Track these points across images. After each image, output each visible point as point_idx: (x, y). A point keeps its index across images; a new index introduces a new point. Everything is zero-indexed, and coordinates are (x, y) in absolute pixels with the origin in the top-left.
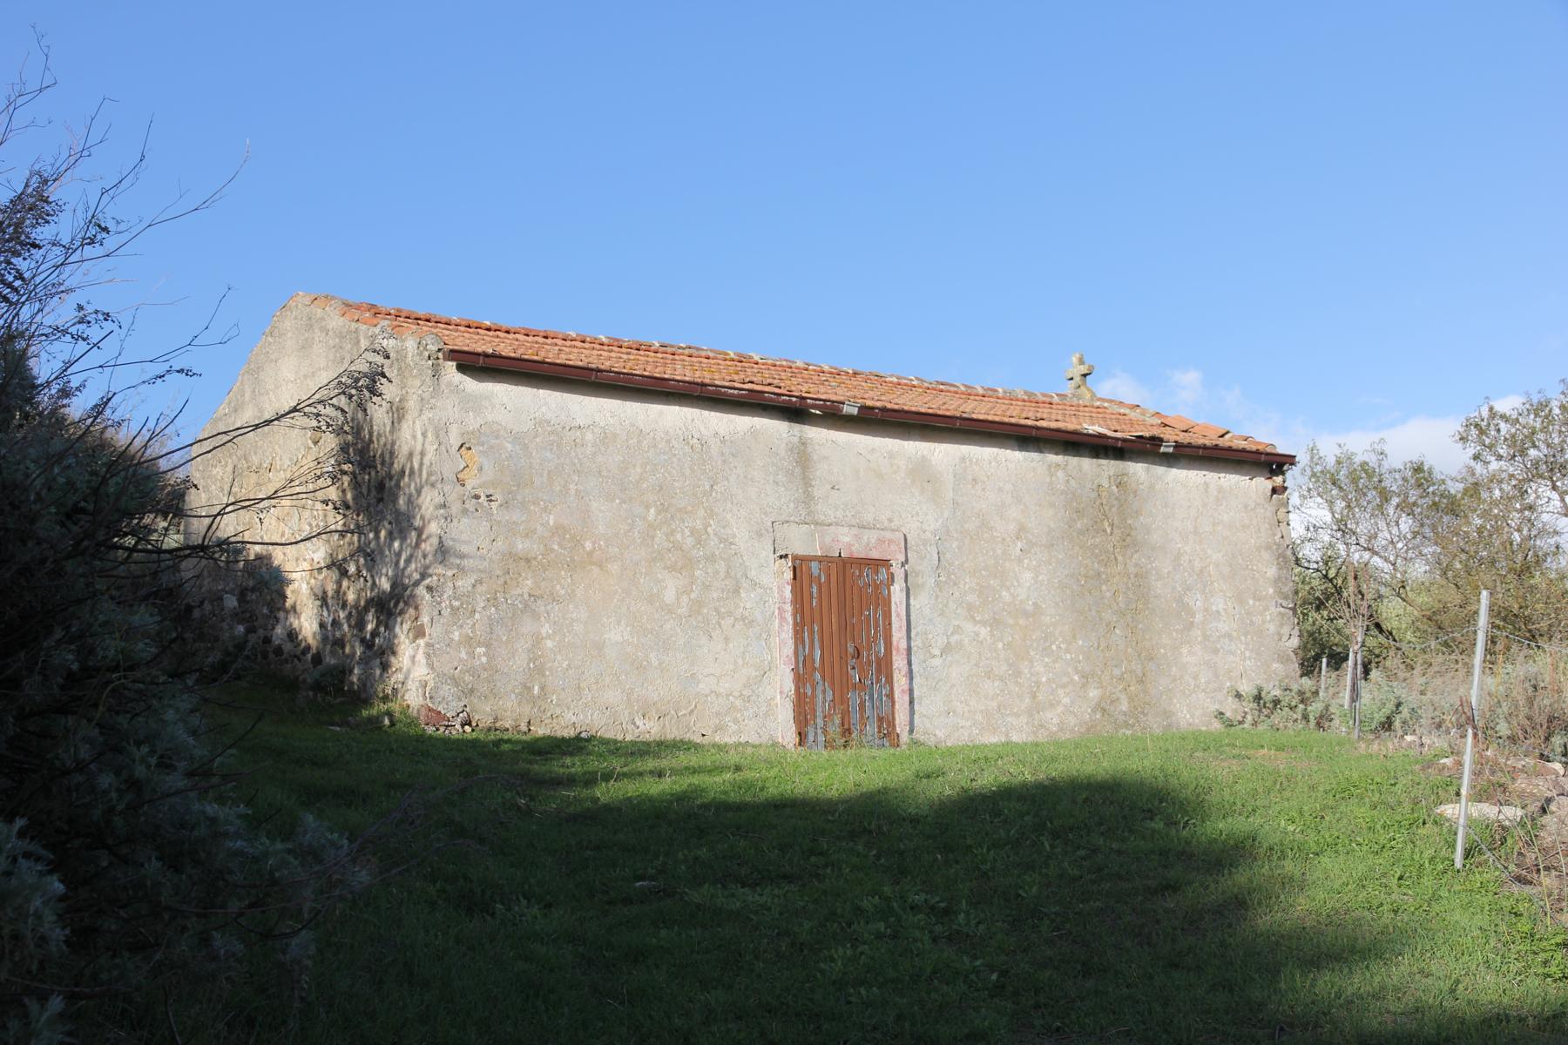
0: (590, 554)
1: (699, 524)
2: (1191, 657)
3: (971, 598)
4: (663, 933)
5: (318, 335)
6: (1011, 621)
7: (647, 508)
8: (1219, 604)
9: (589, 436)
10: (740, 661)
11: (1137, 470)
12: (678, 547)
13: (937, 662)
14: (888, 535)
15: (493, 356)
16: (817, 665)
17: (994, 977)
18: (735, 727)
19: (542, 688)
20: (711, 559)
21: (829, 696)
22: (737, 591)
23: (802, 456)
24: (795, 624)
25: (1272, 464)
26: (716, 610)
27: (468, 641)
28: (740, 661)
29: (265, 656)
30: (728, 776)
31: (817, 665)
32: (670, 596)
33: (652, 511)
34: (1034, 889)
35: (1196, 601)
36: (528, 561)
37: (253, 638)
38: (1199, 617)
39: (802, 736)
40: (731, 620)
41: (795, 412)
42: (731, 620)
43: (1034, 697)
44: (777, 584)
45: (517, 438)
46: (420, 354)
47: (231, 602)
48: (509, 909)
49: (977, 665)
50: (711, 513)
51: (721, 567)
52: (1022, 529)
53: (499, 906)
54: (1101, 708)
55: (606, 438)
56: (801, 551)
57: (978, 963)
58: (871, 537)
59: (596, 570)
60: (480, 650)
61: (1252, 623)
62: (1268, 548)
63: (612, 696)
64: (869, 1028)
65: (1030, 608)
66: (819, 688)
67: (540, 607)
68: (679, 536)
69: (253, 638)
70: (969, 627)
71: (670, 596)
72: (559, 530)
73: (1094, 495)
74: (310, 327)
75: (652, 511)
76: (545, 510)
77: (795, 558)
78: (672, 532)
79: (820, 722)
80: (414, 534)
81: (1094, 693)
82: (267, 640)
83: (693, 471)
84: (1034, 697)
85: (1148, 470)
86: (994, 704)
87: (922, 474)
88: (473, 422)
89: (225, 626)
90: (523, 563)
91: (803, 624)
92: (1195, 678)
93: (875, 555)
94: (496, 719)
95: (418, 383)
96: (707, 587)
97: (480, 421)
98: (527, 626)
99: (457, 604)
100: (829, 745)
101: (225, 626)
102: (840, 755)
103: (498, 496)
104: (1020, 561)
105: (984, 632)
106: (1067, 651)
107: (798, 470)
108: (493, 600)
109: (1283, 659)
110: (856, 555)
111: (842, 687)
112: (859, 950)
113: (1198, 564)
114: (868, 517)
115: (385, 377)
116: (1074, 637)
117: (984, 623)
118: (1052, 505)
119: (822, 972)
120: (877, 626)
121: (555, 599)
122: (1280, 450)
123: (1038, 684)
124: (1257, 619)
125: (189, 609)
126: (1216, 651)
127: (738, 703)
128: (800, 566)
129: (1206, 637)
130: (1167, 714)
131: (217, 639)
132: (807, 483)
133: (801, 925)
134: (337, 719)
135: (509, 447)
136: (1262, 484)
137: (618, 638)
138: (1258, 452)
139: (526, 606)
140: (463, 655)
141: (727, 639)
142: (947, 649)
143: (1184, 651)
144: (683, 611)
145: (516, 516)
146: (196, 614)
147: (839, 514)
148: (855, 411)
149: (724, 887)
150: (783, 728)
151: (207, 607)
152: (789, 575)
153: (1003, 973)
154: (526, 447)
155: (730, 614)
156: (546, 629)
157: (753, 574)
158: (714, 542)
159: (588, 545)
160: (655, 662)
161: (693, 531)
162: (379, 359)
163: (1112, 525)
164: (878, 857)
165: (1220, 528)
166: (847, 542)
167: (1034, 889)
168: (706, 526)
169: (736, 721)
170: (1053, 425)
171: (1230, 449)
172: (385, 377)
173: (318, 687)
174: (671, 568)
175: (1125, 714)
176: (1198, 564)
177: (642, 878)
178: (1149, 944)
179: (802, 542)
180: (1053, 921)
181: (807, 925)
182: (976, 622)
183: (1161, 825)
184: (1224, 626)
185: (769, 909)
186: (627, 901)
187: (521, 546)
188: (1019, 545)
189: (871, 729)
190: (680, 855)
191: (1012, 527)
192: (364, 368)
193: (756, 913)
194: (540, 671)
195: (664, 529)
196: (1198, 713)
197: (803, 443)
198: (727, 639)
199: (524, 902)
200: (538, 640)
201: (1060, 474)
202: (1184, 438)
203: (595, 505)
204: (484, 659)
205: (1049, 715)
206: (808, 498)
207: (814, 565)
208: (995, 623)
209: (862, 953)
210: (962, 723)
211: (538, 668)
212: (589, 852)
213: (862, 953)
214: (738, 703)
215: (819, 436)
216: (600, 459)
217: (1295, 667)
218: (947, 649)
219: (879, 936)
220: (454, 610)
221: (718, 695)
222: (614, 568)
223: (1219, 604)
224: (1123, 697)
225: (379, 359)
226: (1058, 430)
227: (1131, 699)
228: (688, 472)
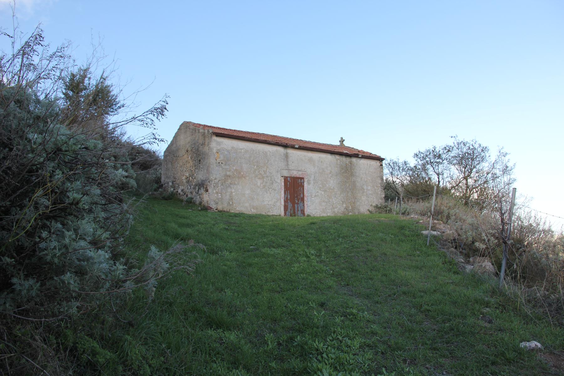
0: (243, 175)
1: (265, 170)
2: (364, 198)
3: (321, 186)
4: (256, 259)
5: (188, 129)
6: (328, 190)
7: (254, 166)
8: (369, 188)
9: (243, 151)
10: (273, 198)
11: (354, 160)
12: (261, 174)
13: (313, 199)
14: (304, 172)
15: (223, 134)
16: (289, 199)
17: (331, 272)
18: (272, 212)
19: (232, 203)
20: (267, 177)
21: (291, 205)
22: (272, 183)
23: (287, 156)
24: (284, 190)
25: (381, 160)
26: (268, 187)
27: (217, 193)
28: (273, 198)
29: (177, 195)
30: (271, 223)
31: (289, 199)
32: (259, 184)
33: (255, 166)
34: (339, 250)
35: (365, 187)
36: (229, 176)
37: (174, 191)
38: (365, 190)
39: (285, 213)
40: (271, 189)
41: (286, 146)
42: (271, 189)
43: (333, 206)
44: (281, 183)
45: (228, 151)
46: (208, 133)
47: (170, 184)
48: (222, 253)
49: (321, 199)
50: (267, 167)
51: (269, 178)
52: (331, 172)
53: (220, 252)
54: (346, 208)
55: (246, 151)
56: (286, 175)
57: (328, 268)
58: (300, 173)
59: (243, 178)
60: (219, 195)
61: (376, 192)
62: (379, 177)
63: (247, 205)
64: (304, 285)
65: (332, 188)
66: (289, 204)
67: (232, 186)
68: (261, 172)
69: (174, 191)
70: (320, 192)
71: (259, 184)
72: (236, 170)
73: (345, 165)
74: (187, 128)
75: (255, 166)
76: (233, 166)
77: (285, 177)
78: (259, 171)
79: (289, 211)
80: (477, 244)
81: (344, 205)
82: (177, 192)
83: (264, 158)
84: (333, 206)
85: (356, 160)
86: (325, 207)
87: (311, 160)
88: (219, 148)
89: (169, 188)
90: (229, 177)
91: (286, 190)
92: (365, 203)
93: (301, 176)
94: (223, 209)
95: (207, 139)
96: (266, 182)
97: (220, 147)
98: (229, 190)
99: (215, 185)
100: (291, 215)
101: (169, 188)
102: (294, 218)
103: (224, 163)
104: (330, 178)
105: (323, 193)
106: (339, 197)
107: (286, 159)
108: (222, 185)
109: (381, 199)
110: (297, 177)
111: (293, 203)
112: (301, 264)
113: (365, 180)
114: (300, 169)
115: (166, 109)
116: (341, 194)
117: (323, 191)
118: (337, 167)
119: (292, 270)
120: (301, 191)
121: (235, 184)
122: (382, 157)
123: (333, 203)
124: (377, 191)
125: (162, 185)
126: (369, 197)
127: (272, 206)
128: (286, 179)
129: (367, 194)
130: (359, 210)
131: (168, 191)
132: (287, 161)
133: (287, 258)
134: (190, 208)
135: (226, 153)
136: (377, 163)
137: (248, 193)
138: (378, 157)
139: (229, 186)
140: (216, 195)
141: (270, 193)
142: (315, 196)
143: (362, 197)
144: (262, 187)
145: (227, 167)
146: (164, 186)
147: (294, 168)
148: (297, 147)
149: (270, 248)
150: (283, 213)
151: (166, 185)
152: (283, 180)
153: (333, 271)
154: (230, 153)
155: (271, 188)
156: (233, 191)
157: (276, 180)
158: (268, 173)
159: (242, 173)
160: (256, 198)
161: (264, 171)
162: (165, 104)
163: (349, 171)
164: (303, 242)
165: (370, 173)
166: (295, 174)
167: (339, 250)
168: (267, 170)
169: (272, 210)
170: (338, 151)
171: (372, 157)
172: (166, 109)
173: (187, 201)
174: (259, 178)
175: (350, 210)
176: (365, 180)
177: (252, 246)
178: (366, 264)
179: (286, 174)
180: (344, 258)
181: (289, 258)
182: (321, 191)
183: (365, 236)
184: (370, 192)
185: (280, 254)
186: (248, 251)
187: (228, 173)
188: (330, 175)
189: (300, 212)
190: (260, 241)
191: (329, 171)
192: (159, 106)
193: (277, 255)
194: (232, 199)
195: (258, 170)
196: (365, 210)
197: (287, 153)
198: (270, 193)
199: (225, 251)
200: (232, 193)
201: (339, 161)
202: (363, 154)
203: (244, 165)
204: (220, 197)
205: (336, 210)
206: (288, 165)
207: (289, 179)
208: (325, 191)
209: (301, 265)
210: (318, 211)
211: (231, 199)
212: (240, 239)
213: (301, 265)
214: (272, 206)
215: (290, 151)
216: (245, 155)
217: (384, 200)
218: (315, 196)
219: (305, 261)
220: (214, 186)
221: (268, 205)
222: (247, 178)
223: (369, 188)
224: (350, 206)
225: (165, 104)
226: (338, 152)
227: (352, 207)
228: (263, 158)
